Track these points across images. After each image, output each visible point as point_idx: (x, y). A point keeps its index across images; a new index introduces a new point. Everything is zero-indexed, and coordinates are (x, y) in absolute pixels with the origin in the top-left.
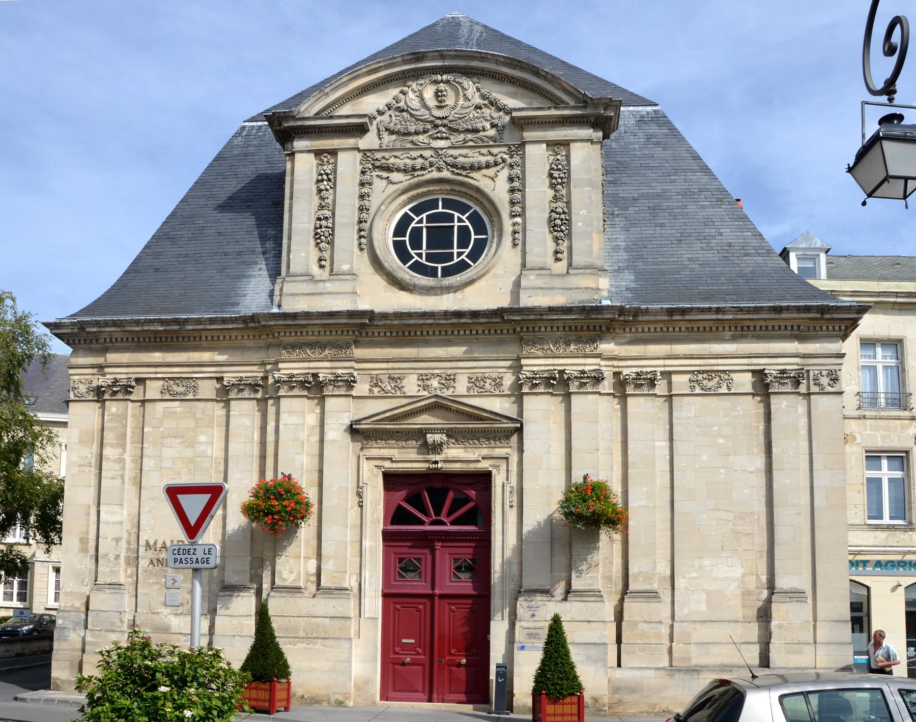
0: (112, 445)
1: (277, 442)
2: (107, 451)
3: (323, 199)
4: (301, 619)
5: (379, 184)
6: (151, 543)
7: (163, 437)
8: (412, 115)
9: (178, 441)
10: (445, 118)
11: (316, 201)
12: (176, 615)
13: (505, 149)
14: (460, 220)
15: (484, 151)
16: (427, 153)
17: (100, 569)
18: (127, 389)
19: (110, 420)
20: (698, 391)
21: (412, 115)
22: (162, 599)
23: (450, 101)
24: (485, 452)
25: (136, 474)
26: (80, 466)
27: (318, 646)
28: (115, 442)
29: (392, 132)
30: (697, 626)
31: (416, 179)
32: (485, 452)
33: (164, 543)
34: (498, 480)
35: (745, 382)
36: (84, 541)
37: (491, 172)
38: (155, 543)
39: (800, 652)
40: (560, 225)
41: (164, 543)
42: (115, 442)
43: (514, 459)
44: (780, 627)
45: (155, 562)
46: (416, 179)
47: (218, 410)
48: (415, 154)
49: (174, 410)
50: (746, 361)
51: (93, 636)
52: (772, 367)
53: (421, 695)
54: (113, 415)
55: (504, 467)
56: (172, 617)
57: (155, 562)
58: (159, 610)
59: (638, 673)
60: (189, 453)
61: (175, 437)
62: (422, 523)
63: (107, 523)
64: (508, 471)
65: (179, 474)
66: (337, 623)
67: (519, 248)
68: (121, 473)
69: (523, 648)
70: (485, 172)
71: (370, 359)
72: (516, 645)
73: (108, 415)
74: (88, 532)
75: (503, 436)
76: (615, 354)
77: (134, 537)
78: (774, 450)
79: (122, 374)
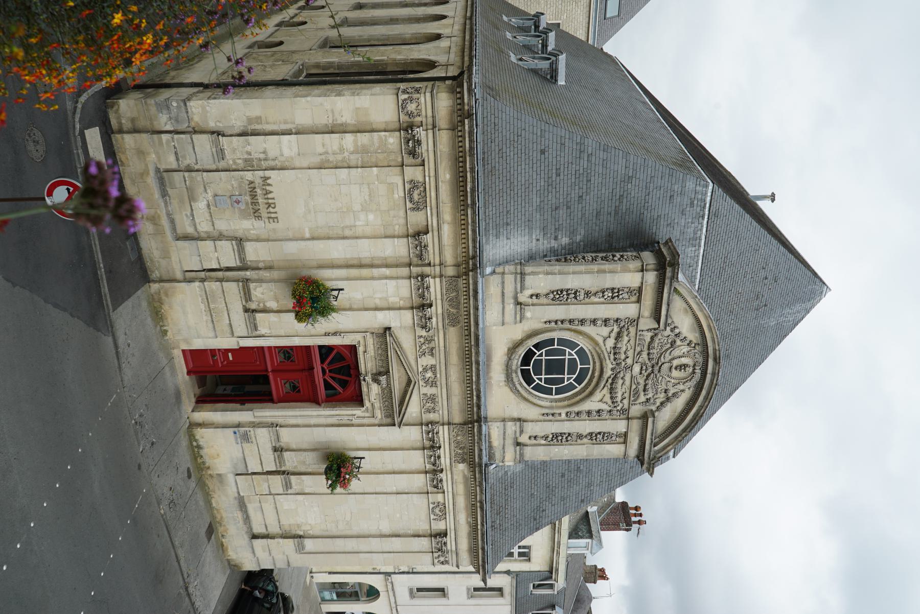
0: (355, 142)
1: (373, 278)
2: (349, 137)
3: (595, 294)
4: (224, 305)
5: (605, 331)
6: (268, 181)
7: (369, 184)
8: (667, 350)
9: (367, 198)
10: (659, 371)
11: (594, 290)
12: (208, 206)
13: (626, 406)
14: (570, 354)
15: (627, 395)
16: (629, 361)
17: (235, 139)
18: (413, 153)
19: (380, 138)
20: (431, 506)
21: (667, 350)
22: (220, 193)
23: (675, 373)
24: (377, 405)
25: (332, 162)
26: (332, 111)
27: (205, 318)
28: (359, 144)
29: (652, 338)
30: (273, 506)
31: (606, 355)
32: (377, 405)
33: (271, 192)
34: (358, 412)
35: (440, 526)
36: (258, 120)
37: (607, 398)
38: (269, 185)
39: (264, 551)
40: (557, 438)
41: (271, 192)
42: (359, 144)
43: (372, 421)
44: (278, 543)
45: (252, 185)
46: (606, 355)
47: (398, 229)
48: (630, 354)
49: (395, 192)
50: (453, 527)
51: (168, 141)
52: (450, 540)
53: (191, 366)
54: (386, 140)
55: (367, 415)
56: (205, 202)
57: (252, 185)
58: (209, 191)
59: (233, 484)
60: (357, 207)
61: (370, 195)
62: (322, 361)
63: (280, 142)
64: (364, 417)
65: (336, 200)
66: (227, 329)
67: (542, 418)
68: (330, 152)
69: (235, 433)
70: (608, 396)
71: (449, 340)
72: (236, 429)
73: (385, 136)
74: (268, 123)
75: (390, 415)
76: (456, 476)
77: (272, 163)
78: (394, 539)
79: (427, 147)
